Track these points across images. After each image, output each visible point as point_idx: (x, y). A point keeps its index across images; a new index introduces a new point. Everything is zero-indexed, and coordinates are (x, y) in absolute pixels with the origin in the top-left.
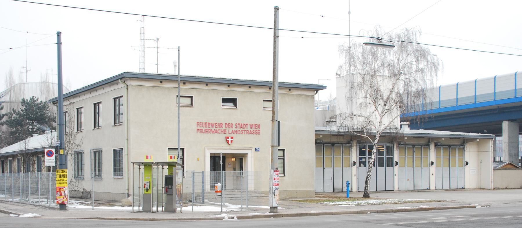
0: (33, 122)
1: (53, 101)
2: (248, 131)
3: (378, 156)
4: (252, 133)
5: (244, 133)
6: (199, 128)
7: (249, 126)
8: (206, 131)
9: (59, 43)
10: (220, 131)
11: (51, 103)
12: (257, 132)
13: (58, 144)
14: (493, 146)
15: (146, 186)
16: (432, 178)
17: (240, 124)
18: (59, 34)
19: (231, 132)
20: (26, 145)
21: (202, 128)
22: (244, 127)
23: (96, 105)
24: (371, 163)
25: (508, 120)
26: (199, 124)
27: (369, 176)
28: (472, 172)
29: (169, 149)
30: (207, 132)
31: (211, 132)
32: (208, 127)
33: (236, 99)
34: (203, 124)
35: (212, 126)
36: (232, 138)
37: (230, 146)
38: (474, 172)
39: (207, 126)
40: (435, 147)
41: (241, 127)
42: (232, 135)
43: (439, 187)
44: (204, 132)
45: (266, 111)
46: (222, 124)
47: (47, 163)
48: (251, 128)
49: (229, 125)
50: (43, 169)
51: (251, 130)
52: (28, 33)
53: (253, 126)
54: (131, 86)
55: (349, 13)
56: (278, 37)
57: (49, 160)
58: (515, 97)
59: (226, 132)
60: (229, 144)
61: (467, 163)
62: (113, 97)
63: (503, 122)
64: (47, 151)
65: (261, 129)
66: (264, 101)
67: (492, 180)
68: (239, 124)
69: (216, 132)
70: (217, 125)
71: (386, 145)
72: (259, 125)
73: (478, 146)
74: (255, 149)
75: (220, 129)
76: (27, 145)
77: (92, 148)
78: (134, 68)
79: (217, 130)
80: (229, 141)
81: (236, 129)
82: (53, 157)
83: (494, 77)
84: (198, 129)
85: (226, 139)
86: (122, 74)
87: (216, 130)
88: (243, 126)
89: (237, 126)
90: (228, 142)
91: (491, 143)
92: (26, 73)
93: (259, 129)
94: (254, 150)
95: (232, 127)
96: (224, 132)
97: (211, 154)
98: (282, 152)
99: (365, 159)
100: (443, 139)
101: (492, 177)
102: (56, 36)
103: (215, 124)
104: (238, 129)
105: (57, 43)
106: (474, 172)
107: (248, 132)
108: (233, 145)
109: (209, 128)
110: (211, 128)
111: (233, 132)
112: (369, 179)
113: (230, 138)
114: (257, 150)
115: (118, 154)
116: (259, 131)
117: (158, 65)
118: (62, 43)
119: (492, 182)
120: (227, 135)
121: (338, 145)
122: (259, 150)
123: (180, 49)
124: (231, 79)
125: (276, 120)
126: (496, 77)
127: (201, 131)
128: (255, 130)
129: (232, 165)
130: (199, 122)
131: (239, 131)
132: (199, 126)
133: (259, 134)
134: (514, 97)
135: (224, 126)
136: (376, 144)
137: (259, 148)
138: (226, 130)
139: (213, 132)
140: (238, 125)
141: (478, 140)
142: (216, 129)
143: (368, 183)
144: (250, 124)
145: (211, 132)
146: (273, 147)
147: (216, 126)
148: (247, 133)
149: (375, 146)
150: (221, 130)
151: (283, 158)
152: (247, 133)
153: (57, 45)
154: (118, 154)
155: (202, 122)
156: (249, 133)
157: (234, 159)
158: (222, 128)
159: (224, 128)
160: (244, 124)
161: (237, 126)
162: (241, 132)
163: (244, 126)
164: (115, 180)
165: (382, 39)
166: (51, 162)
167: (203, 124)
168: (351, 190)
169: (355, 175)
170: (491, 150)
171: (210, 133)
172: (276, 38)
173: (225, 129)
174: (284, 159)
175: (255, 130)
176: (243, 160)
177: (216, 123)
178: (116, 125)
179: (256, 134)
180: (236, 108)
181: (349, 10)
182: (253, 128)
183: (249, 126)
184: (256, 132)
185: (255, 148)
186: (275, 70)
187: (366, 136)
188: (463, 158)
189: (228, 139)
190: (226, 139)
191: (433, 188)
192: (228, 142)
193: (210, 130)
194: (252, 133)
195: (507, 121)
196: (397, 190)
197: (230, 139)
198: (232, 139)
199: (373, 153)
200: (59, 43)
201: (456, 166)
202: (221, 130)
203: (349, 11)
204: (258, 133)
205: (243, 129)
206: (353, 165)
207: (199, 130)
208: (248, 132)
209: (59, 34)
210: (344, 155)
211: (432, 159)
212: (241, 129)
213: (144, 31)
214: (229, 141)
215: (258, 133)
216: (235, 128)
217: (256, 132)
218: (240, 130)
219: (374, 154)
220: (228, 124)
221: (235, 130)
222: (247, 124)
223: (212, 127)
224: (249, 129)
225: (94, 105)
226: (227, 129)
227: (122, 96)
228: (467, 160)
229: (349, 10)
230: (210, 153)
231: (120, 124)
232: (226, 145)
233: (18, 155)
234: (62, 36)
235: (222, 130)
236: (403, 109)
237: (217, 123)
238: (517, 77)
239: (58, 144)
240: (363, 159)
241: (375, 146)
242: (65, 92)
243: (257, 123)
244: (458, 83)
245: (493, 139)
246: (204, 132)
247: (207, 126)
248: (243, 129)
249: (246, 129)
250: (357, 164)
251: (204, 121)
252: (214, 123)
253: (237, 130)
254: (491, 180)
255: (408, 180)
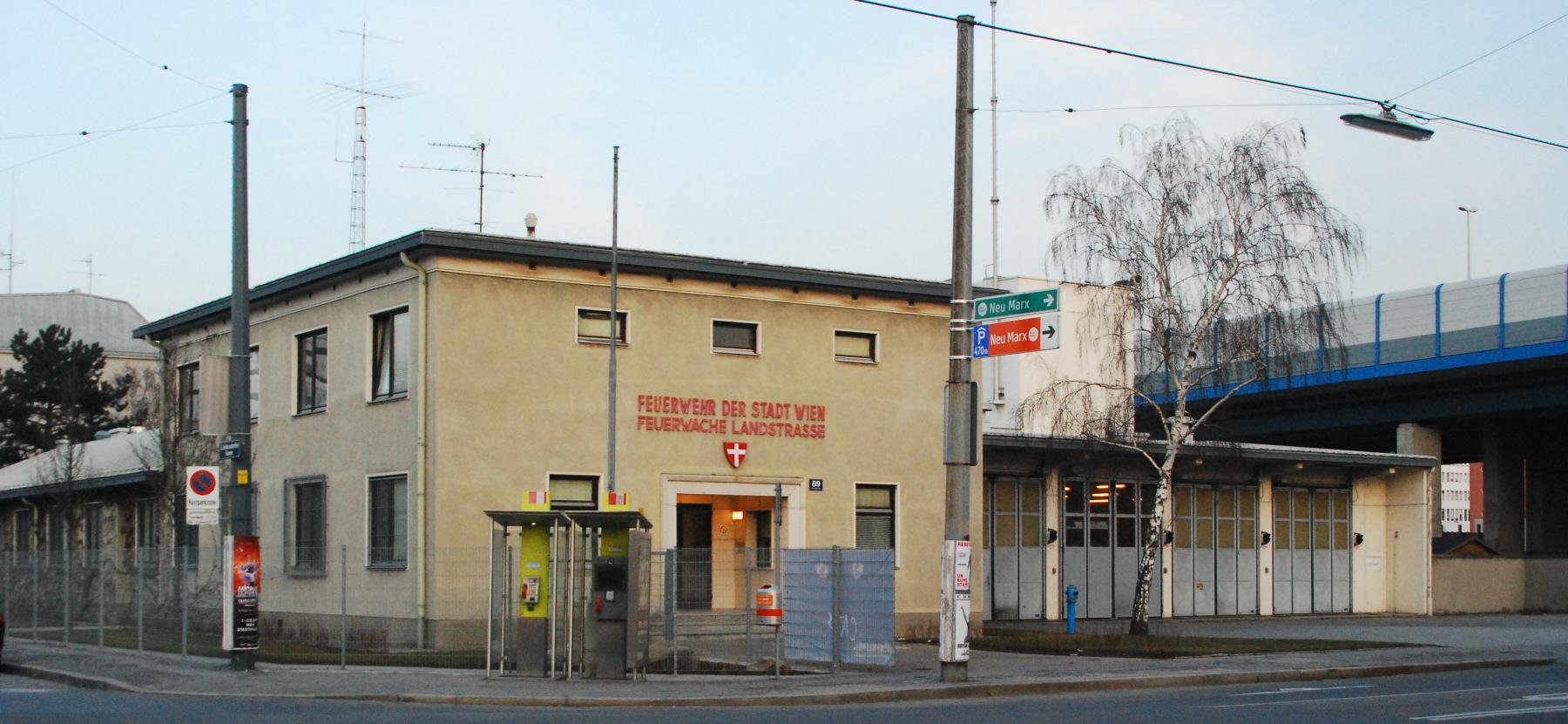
0: (50, 405)
1: (153, 330)
2: (789, 425)
3: (1118, 513)
4: (802, 432)
5: (777, 432)
6: (644, 413)
7: (792, 411)
8: (666, 426)
9: (240, 123)
10: (706, 426)
11: (146, 337)
12: (817, 429)
13: (229, 450)
14: (1431, 488)
15: (528, 592)
16: (1266, 580)
17: (766, 404)
18: (240, 92)
19: (739, 428)
20: (73, 463)
21: (653, 414)
22: (780, 414)
23: (383, 322)
24: (1155, 531)
25: (1414, 422)
26: (644, 400)
27: (1149, 572)
28: (1371, 564)
29: (553, 477)
30: (668, 427)
31: (681, 428)
32: (671, 410)
33: (756, 325)
34: (658, 402)
35: (685, 407)
36: (743, 446)
37: (739, 472)
38: (1376, 564)
39: (650, 407)
40: (1272, 490)
41: (770, 414)
42: (744, 438)
43: (1284, 608)
44: (659, 425)
45: (847, 367)
46: (712, 401)
47: (193, 515)
48: (800, 417)
49: (735, 408)
50: (109, 542)
51: (798, 425)
52: (163, 65)
53: (806, 410)
54: (438, 275)
55: (992, 101)
56: (972, 111)
57: (204, 502)
58: (1502, 347)
59: (725, 427)
60: (734, 467)
61: (1359, 539)
62: (297, 333)
63: (1398, 426)
64: (196, 475)
65: (829, 423)
66: (838, 334)
67: (1430, 589)
68: (764, 404)
69: (697, 427)
70: (697, 407)
71: (1140, 483)
72: (824, 407)
73: (1387, 490)
74: (808, 482)
75: (709, 418)
76: (76, 464)
77: (290, 475)
78: (456, 219)
79: (699, 422)
80: (733, 456)
81: (754, 420)
82: (215, 495)
83: (1498, 280)
84: (641, 418)
85: (726, 452)
86: (417, 235)
87: (696, 420)
88: (775, 412)
89: (756, 410)
90: (730, 459)
91: (1425, 480)
92: (10, 269)
93: (823, 420)
94: (805, 485)
95: (742, 413)
96: (720, 427)
97: (679, 495)
98: (887, 493)
99: (1080, 523)
100: (1199, 462)
101: (1428, 580)
102: (229, 101)
103: (692, 403)
104: (760, 420)
105: (232, 123)
106: (1376, 564)
107: (789, 428)
108: (748, 469)
109: (675, 416)
110: (680, 415)
111: (745, 430)
112: (1147, 578)
113: (737, 446)
114: (815, 486)
115: (384, 490)
116: (823, 427)
117: (481, 224)
118: (250, 123)
119: (1430, 594)
120: (730, 438)
121: (1005, 479)
122: (821, 486)
123: (619, 155)
124: (743, 262)
125: (965, 379)
126: (1382, 299)
127: (651, 424)
128: (810, 423)
129: (729, 534)
130: (646, 393)
131: (764, 425)
132: (644, 408)
133: (823, 437)
134: (1497, 347)
135: (718, 409)
136: (1168, 474)
137: (821, 481)
138: (724, 422)
139: (686, 428)
140: (760, 408)
141: (1392, 471)
142: (694, 417)
143: (1144, 591)
144: (796, 406)
145: (681, 428)
146: (951, 467)
147: (697, 410)
148: (788, 432)
149: (1164, 480)
150: (711, 421)
151: (890, 511)
152: (788, 432)
153: (232, 126)
154: (384, 490)
155: (654, 395)
156: (792, 433)
157: (738, 515)
158: (714, 414)
159: (719, 416)
160: (779, 405)
161: (756, 410)
162: (769, 430)
163: (782, 414)
164: (376, 576)
165: (1394, 107)
166: (207, 511)
167: (658, 402)
168: (1043, 615)
169: (1054, 571)
170: (1425, 502)
171: (678, 430)
172: (965, 116)
173: (723, 418)
174: (892, 516)
175: (810, 423)
176: (770, 516)
177: (697, 400)
178: (378, 399)
179: (812, 436)
180: (753, 354)
181: (994, 93)
182: (805, 418)
183: (792, 411)
184: (814, 432)
185: (811, 481)
186: (962, 219)
187: (1135, 448)
188: (1307, 523)
189: (730, 451)
190: (726, 452)
191: (1167, 613)
192: (730, 459)
193: (677, 420)
194: (802, 432)
195: (1410, 424)
196: (1271, 613)
197: (736, 452)
198: (743, 452)
199: (1159, 500)
200: (240, 123)
201: (1346, 548)
202: (711, 421)
203: (991, 95)
204: (819, 433)
205: (776, 421)
206: (1048, 539)
207: (645, 421)
208: (792, 432)
209: (240, 92)
210: (999, 510)
211: (1266, 523)
212: (769, 421)
213: (365, 152)
214: (733, 456)
215: (819, 433)
216: (752, 415)
217: (814, 432)
218: (768, 424)
219: (1161, 503)
220: (730, 403)
221: (751, 423)
222: (787, 406)
223: (684, 412)
224: (793, 421)
225: (297, 341)
226: (729, 419)
227: (405, 309)
228: (1357, 528)
229: (994, 93)
230: (678, 494)
231: (392, 398)
232: (727, 469)
233: (24, 500)
234: (250, 96)
235: (714, 423)
236: (1261, 368)
237: (700, 398)
238: (1507, 288)
239: (229, 450)
240: (1076, 523)
241: (1164, 480)
242: (257, 278)
243: (816, 404)
244: (1441, 286)
245: (1431, 468)
246: (659, 425)
247: (652, 407)
248: (776, 421)
249: (783, 421)
250: (1062, 536)
251: (659, 392)
252: (690, 400)
253: (757, 423)
254: (1425, 587)
255: (1200, 586)
